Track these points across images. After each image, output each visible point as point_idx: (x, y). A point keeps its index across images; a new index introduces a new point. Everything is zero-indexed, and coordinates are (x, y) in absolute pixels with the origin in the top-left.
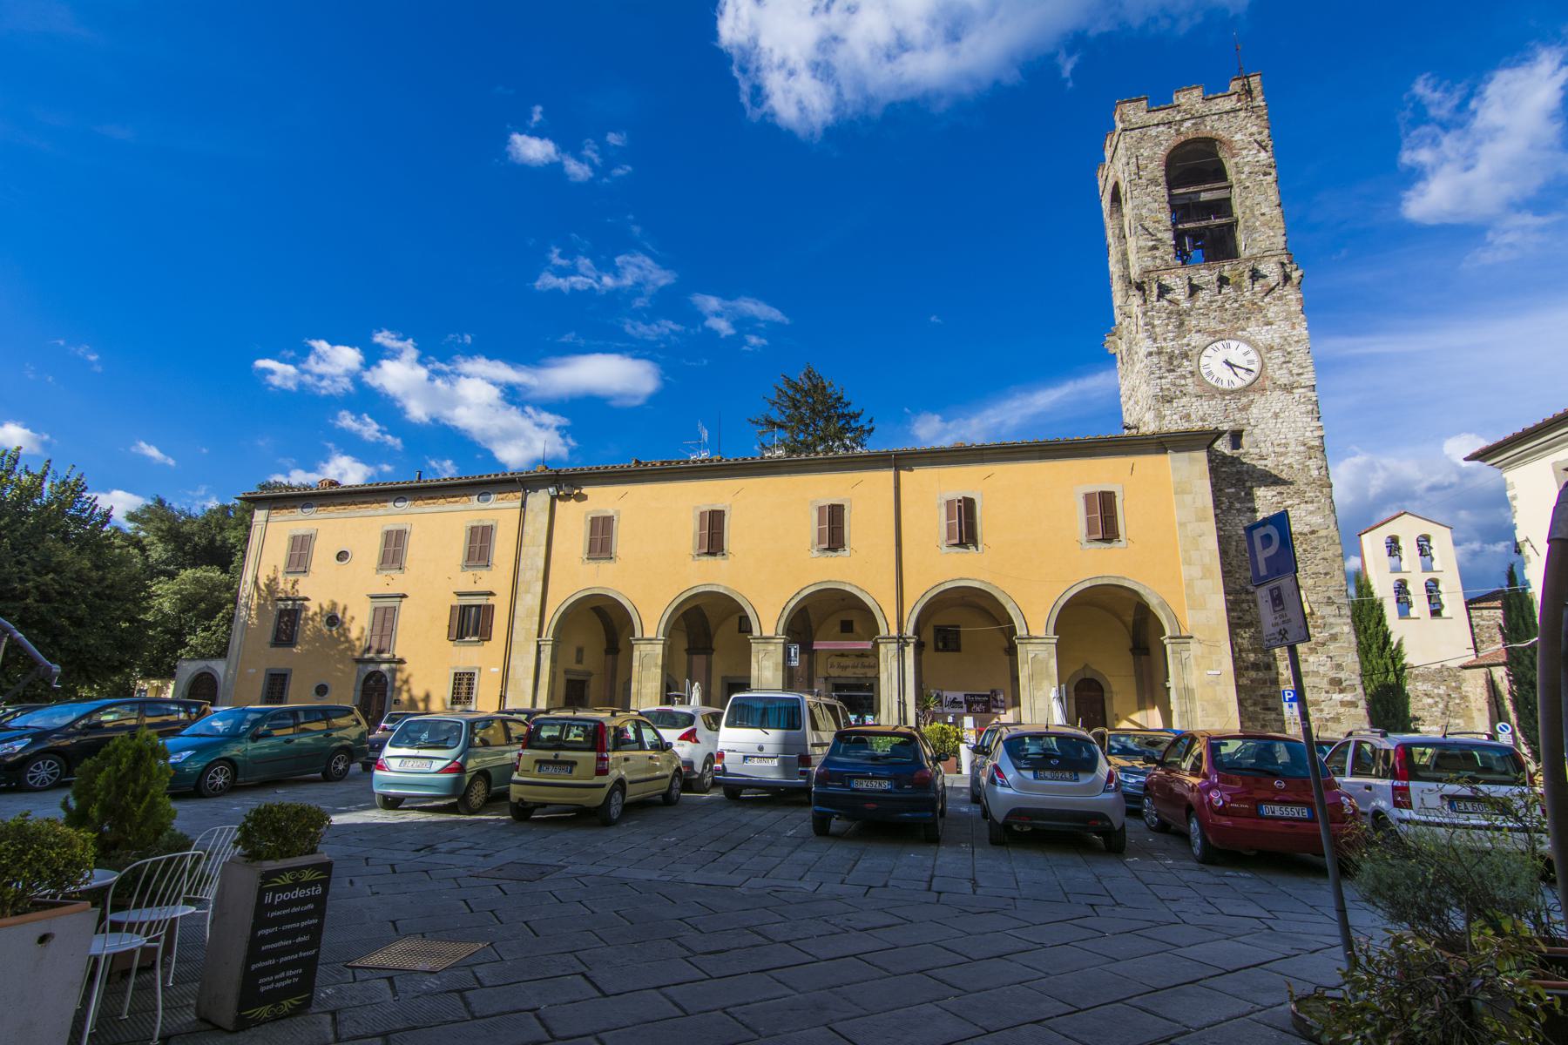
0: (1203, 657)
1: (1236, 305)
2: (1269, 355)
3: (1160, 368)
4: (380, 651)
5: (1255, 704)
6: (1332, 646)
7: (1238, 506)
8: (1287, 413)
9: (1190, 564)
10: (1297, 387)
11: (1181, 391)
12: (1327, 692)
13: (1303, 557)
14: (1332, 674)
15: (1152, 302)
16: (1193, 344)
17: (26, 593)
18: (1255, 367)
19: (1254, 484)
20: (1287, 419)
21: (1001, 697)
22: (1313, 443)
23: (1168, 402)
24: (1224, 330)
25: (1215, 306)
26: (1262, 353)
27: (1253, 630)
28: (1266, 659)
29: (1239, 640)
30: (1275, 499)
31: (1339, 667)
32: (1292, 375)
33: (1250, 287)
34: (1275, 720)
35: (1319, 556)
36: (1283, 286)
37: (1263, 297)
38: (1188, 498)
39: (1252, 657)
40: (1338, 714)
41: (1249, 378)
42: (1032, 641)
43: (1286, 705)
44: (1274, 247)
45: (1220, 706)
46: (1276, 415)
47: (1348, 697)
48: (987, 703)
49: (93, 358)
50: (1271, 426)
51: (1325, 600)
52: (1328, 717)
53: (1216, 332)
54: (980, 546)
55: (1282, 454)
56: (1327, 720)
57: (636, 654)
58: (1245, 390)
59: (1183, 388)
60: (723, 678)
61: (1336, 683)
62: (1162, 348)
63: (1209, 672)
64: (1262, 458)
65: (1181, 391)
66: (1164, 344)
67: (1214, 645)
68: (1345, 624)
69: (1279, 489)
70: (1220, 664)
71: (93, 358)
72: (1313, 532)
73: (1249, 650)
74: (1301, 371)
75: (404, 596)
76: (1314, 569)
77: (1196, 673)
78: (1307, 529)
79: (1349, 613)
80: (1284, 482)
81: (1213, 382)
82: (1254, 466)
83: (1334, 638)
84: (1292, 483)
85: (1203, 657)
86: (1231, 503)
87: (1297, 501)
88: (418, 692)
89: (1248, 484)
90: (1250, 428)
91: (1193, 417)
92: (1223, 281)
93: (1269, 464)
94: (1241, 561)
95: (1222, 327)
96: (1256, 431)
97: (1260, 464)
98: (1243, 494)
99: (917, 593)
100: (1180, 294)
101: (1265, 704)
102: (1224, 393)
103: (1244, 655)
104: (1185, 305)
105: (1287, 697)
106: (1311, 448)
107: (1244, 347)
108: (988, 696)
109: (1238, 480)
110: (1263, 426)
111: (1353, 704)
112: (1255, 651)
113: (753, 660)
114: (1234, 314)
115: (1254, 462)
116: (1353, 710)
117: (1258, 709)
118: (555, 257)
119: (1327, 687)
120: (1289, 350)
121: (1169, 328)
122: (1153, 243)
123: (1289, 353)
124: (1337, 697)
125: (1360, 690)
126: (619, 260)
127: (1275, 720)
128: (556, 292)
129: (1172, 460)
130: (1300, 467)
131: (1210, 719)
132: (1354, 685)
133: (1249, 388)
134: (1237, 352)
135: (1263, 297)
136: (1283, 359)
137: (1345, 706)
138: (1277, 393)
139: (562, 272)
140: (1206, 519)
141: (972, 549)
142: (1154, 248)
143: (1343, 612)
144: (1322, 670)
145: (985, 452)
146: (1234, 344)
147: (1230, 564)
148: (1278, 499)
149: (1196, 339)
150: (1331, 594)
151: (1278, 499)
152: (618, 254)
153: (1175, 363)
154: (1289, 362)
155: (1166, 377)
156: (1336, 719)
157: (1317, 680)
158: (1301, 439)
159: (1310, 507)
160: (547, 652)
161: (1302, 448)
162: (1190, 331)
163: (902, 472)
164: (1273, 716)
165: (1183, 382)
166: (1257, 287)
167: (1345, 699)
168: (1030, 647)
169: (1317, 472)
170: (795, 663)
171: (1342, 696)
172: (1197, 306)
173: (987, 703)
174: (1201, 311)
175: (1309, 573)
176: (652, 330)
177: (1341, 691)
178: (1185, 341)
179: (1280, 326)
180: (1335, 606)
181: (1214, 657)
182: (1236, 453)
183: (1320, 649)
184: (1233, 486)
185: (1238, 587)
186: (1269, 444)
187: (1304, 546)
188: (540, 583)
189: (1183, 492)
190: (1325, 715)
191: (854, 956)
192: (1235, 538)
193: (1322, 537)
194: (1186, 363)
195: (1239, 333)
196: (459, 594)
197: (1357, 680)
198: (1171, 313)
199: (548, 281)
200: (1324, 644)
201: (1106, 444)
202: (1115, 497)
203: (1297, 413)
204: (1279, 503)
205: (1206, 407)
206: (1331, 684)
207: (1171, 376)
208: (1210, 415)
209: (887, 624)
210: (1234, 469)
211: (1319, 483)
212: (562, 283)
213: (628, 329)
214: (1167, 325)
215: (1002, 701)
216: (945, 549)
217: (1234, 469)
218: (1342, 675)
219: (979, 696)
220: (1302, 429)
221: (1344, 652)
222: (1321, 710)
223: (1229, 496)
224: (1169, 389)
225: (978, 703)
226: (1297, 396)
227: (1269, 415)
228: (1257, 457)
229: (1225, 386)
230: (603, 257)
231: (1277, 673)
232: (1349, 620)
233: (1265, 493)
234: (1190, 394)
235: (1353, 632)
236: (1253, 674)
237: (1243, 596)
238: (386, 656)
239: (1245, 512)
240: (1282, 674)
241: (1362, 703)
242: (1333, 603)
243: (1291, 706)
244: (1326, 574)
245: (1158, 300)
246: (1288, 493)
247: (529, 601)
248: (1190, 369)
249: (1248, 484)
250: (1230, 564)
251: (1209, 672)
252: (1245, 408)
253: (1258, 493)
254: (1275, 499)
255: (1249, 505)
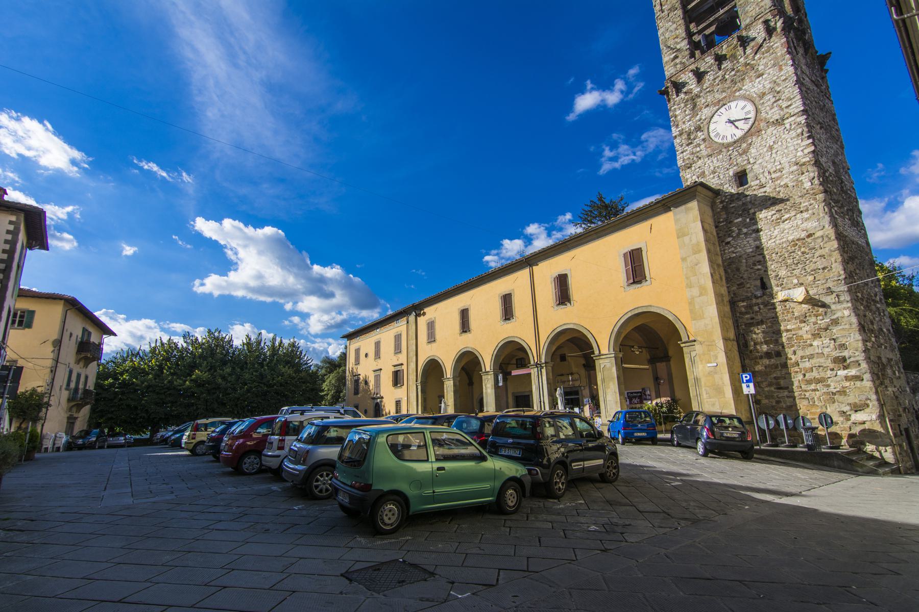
0: (704, 354)
1: (733, 73)
2: (762, 102)
3: (682, 145)
4: (377, 394)
5: (770, 385)
6: (835, 330)
7: (745, 230)
8: (780, 143)
9: (691, 287)
10: (788, 118)
11: (697, 157)
12: (832, 370)
13: (802, 258)
14: (836, 354)
15: (674, 99)
16: (703, 118)
17: (275, 384)
18: (752, 115)
19: (756, 210)
20: (780, 148)
21: (648, 392)
22: (804, 160)
23: (689, 168)
24: (726, 97)
25: (717, 81)
26: (756, 102)
27: (764, 326)
28: (776, 348)
29: (754, 336)
30: (774, 217)
31: (843, 346)
32: (782, 109)
33: (742, 53)
34: (788, 397)
35: (817, 255)
36: (769, 39)
37: (754, 57)
38: (686, 239)
39: (765, 348)
40: (843, 387)
41: (746, 127)
42: (602, 357)
43: (744, 386)
44: (763, 9)
45: (719, 391)
46: (771, 148)
47: (853, 372)
48: (640, 397)
49: (423, 274)
50: (767, 158)
51: (825, 291)
52: (834, 391)
53: (719, 101)
54: (572, 302)
55: (778, 178)
56: (834, 394)
57: (445, 386)
58: (743, 139)
59: (698, 154)
60: (513, 393)
61: (842, 362)
62: (683, 129)
63: (709, 365)
64: (762, 186)
65: (697, 157)
66: (684, 126)
67: (711, 345)
68: (844, 309)
69: (777, 207)
70: (716, 357)
71: (423, 274)
72: (810, 236)
73: (762, 343)
74: (789, 103)
75: (381, 369)
76: (813, 266)
77: (700, 367)
78: (803, 235)
79: (848, 298)
80: (782, 201)
81: (720, 141)
82: (756, 195)
83: (835, 322)
84: (788, 200)
85: (704, 354)
86: (740, 230)
87: (793, 213)
88: (387, 411)
89: (752, 211)
90: (750, 166)
91: (707, 173)
92: (720, 59)
93: (769, 190)
94: (751, 273)
95: (724, 95)
96: (756, 166)
97: (760, 193)
98: (748, 220)
99: (545, 335)
100: (692, 85)
101: (778, 384)
102: (728, 146)
103: (758, 347)
104: (696, 90)
105: (745, 379)
106: (804, 164)
107: (742, 103)
108: (641, 392)
109: (744, 210)
110: (760, 161)
111: (859, 378)
112: (766, 343)
113: (484, 384)
114: (732, 81)
115: (755, 193)
116: (858, 383)
117: (772, 389)
118: (608, 153)
119: (832, 366)
120: (778, 90)
121: (687, 113)
122: (674, 54)
123: (778, 92)
124: (842, 373)
125: (864, 365)
126: (643, 137)
127: (788, 397)
128: (614, 171)
129: (675, 215)
130: (794, 184)
131: (711, 400)
132: (857, 361)
133: (747, 135)
134: (739, 109)
135: (754, 57)
136: (774, 100)
137: (850, 380)
138: (771, 129)
139: (614, 159)
140: (699, 251)
141: (568, 304)
142: (676, 57)
143: (842, 299)
144: (826, 351)
145: (567, 243)
146: (733, 104)
147: (742, 277)
148: (778, 216)
149: (706, 112)
150: (830, 284)
151: (778, 216)
152: (643, 133)
153: (692, 137)
154: (779, 100)
155: (686, 150)
156: (843, 392)
157: (822, 360)
158: (794, 160)
159: (805, 215)
160: (419, 387)
161: (795, 168)
162: (701, 109)
163: (534, 267)
164: (786, 393)
165: (698, 149)
166: (749, 51)
167: (850, 374)
168: (601, 361)
169: (809, 184)
170: (501, 384)
171: (846, 371)
172: (704, 88)
173: (640, 397)
174: (708, 90)
175: (809, 271)
176: (673, 169)
177: (845, 368)
178: (698, 118)
179: (769, 74)
180: (835, 294)
181: (712, 353)
182: (741, 189)
183: (823, 334)
184: (740, 216)
185: (749, 295)
186: (766, 174)
187: (803, 249)
188: (415, 357)
189: (684, 235)
190: (832, 389)
191: (739, 581)
192: (745, 256)
193: (818, 237)
194: (699, 134)
195: (737, 94)
196: (395, 366)
197: (860, 357)
198: (687, 101)
199: (607, 167)
200: (826, 329)
201: (650, 209)
202: (642, 251)
203: (789, 140)
204: (778, 219)
205: (715, 162)
206: (835, 362)
207: (689, 149)
208: (718, 167)
209: (533, 358)
210: (740, 203)
211: (811, 192)
212: (617, 165)
213: (657, 174)
214: (685, 111)
215: (649, 395)
216: (556, 308)
217: (740, 203)
218: (846, 354)
219: (635, 393)
220: (794, 152)
221: (846, 333)
222: (829, 386)
223: (738, 225)
224: (689, 158)
225: (635, 397)
226: (788, 126)
227: (765, 150)
228: (757, 187)
229: (730, 140)
230: (634, 140)
231: (787, 358)
232: (850, 305)
233: (766, 215)
234: (703, 156)
235: (853, 314)
236: (766, 361)
237: (754, 301)
238: (378, 395)
239: (751, 234)
240: (791, 359)
241: (867, 376)
242: (832, 292)
243: (748, 386)
244: (824, 269)
245: (677, 96)
246: (785, 209)
247: (413, 365)
248: (703, 137)
249: (752, 211)
250: (742, 277)
251: (709, 365)
252: (745, 152)
253: (761, 216)
254: (774, 217)
255: (754, 227)
